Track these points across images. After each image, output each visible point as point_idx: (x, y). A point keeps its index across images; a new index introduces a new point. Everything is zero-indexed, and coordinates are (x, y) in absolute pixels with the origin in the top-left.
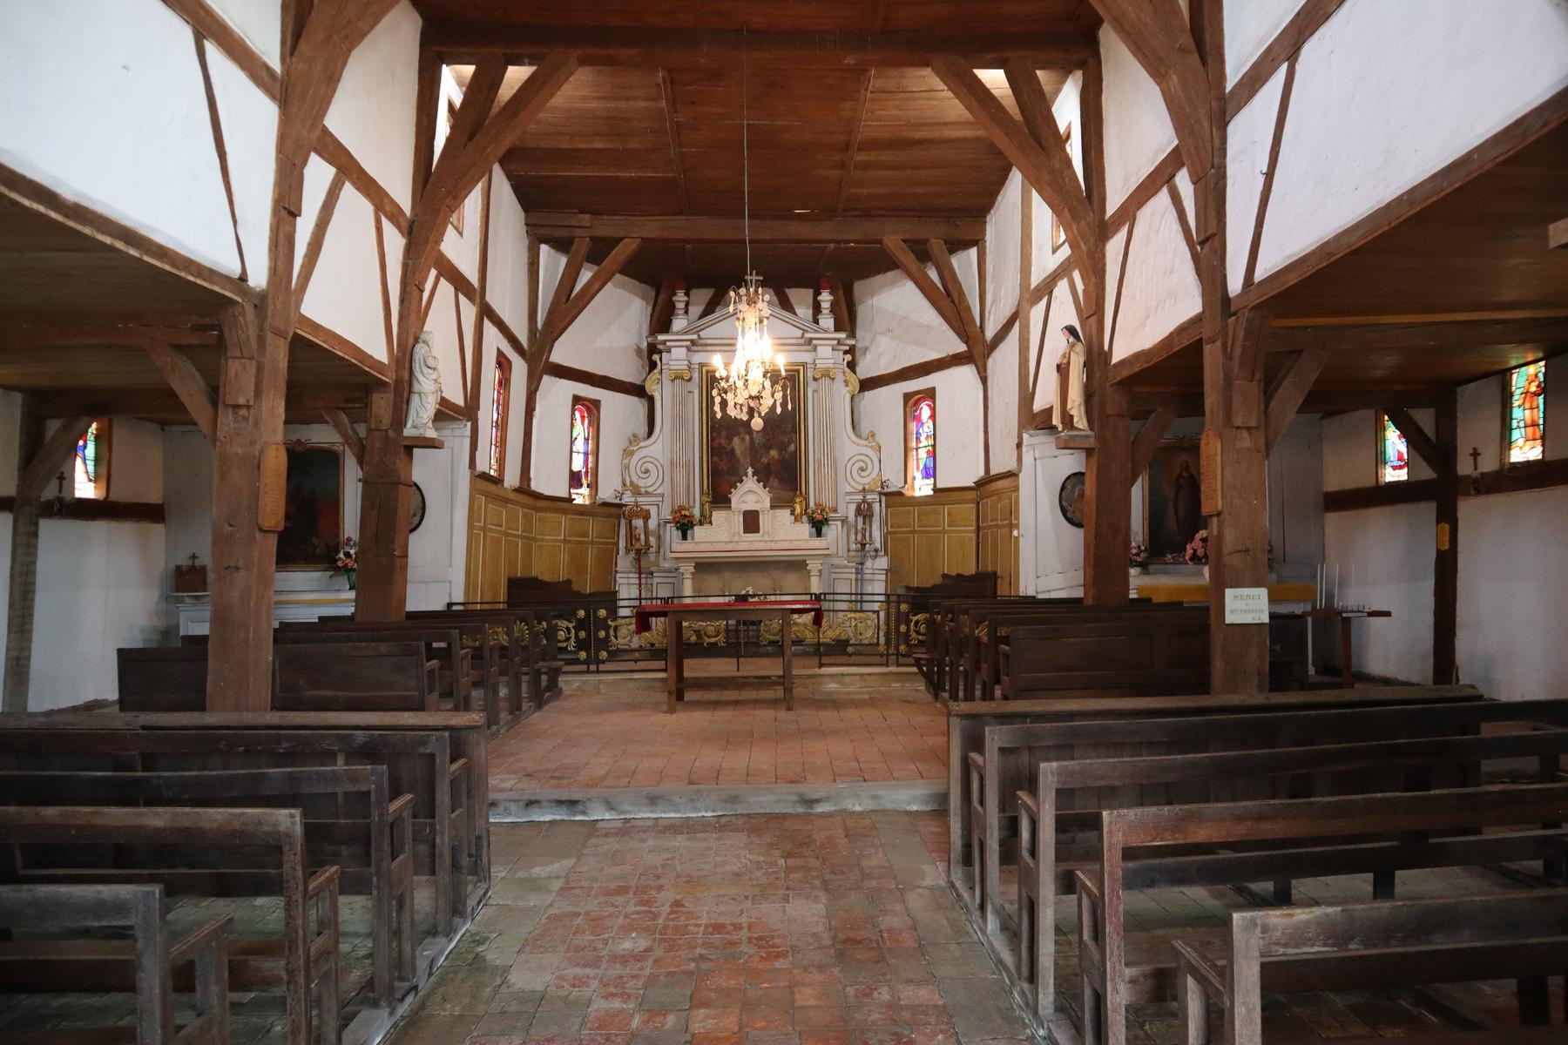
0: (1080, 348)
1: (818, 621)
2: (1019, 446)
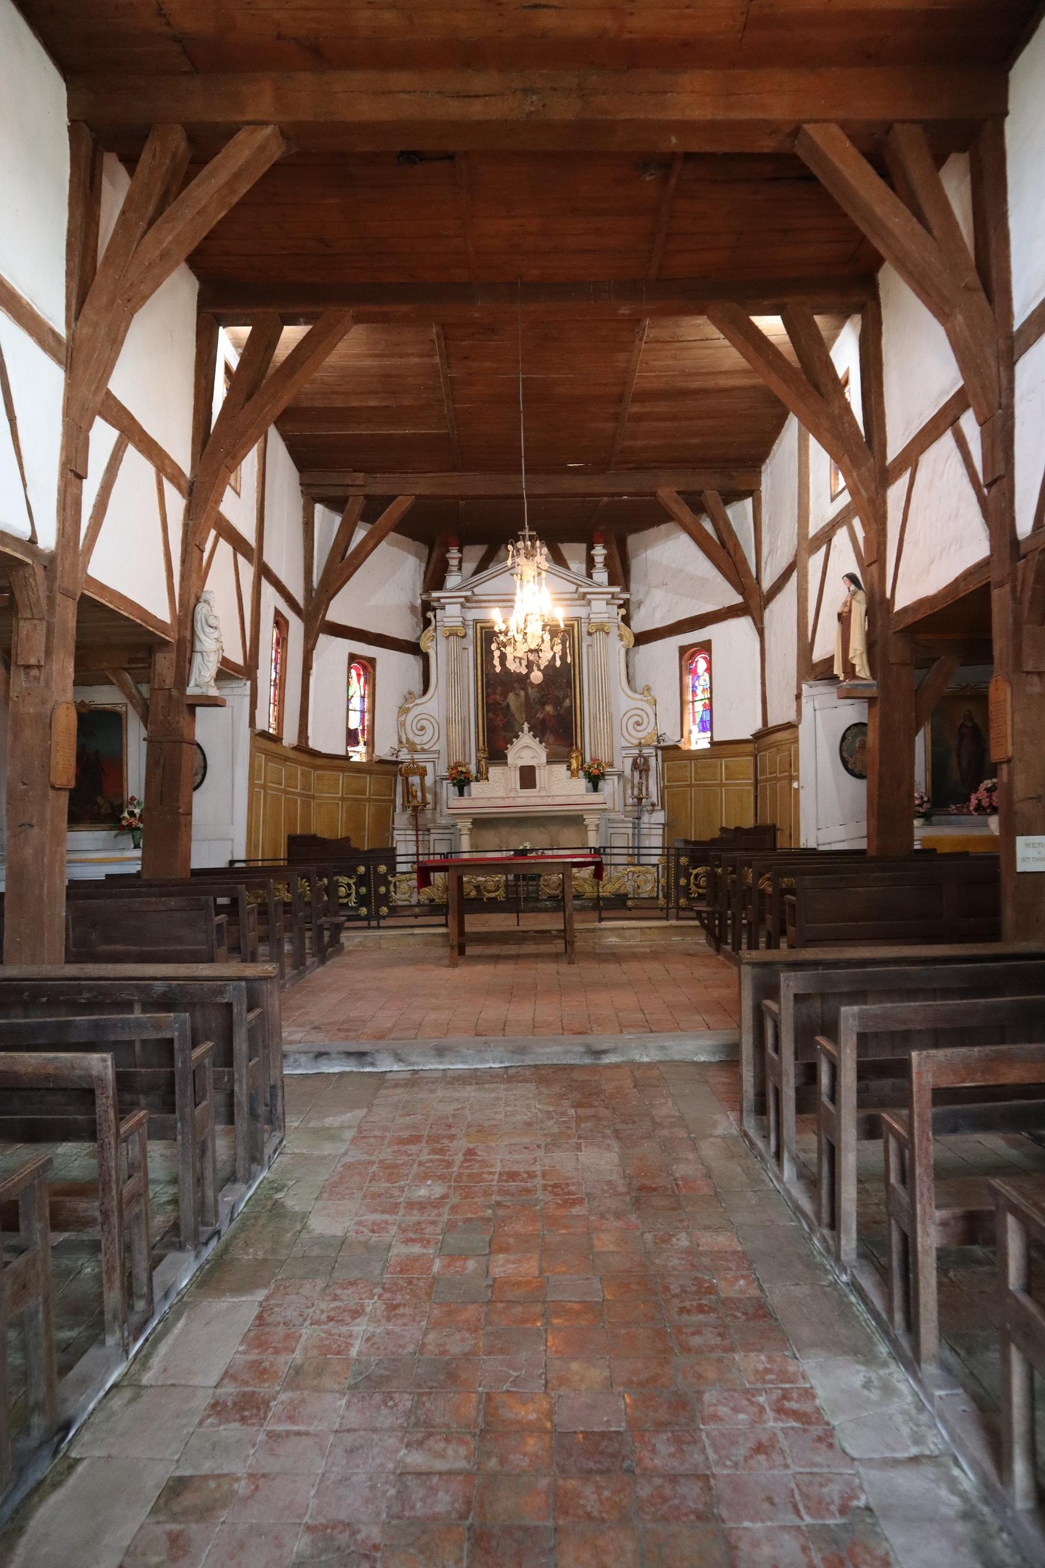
0: (861, 596)
1: (598, 874)
2: (798, 697)
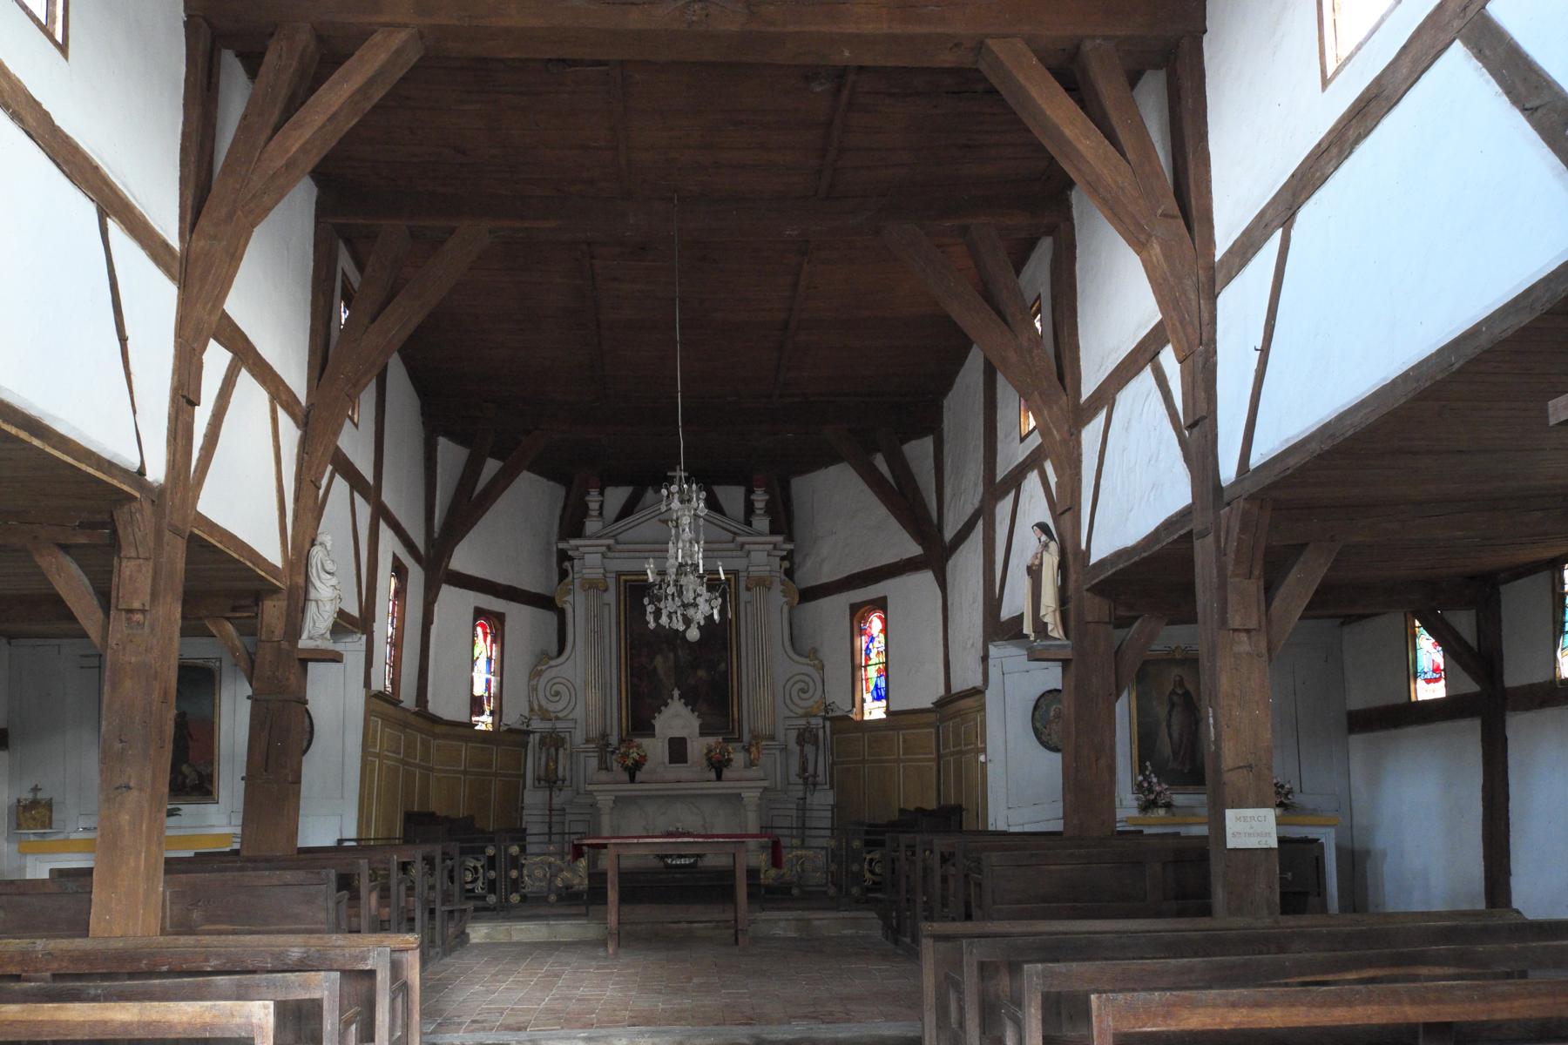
0: (1053, 546)
2: (985, 658)
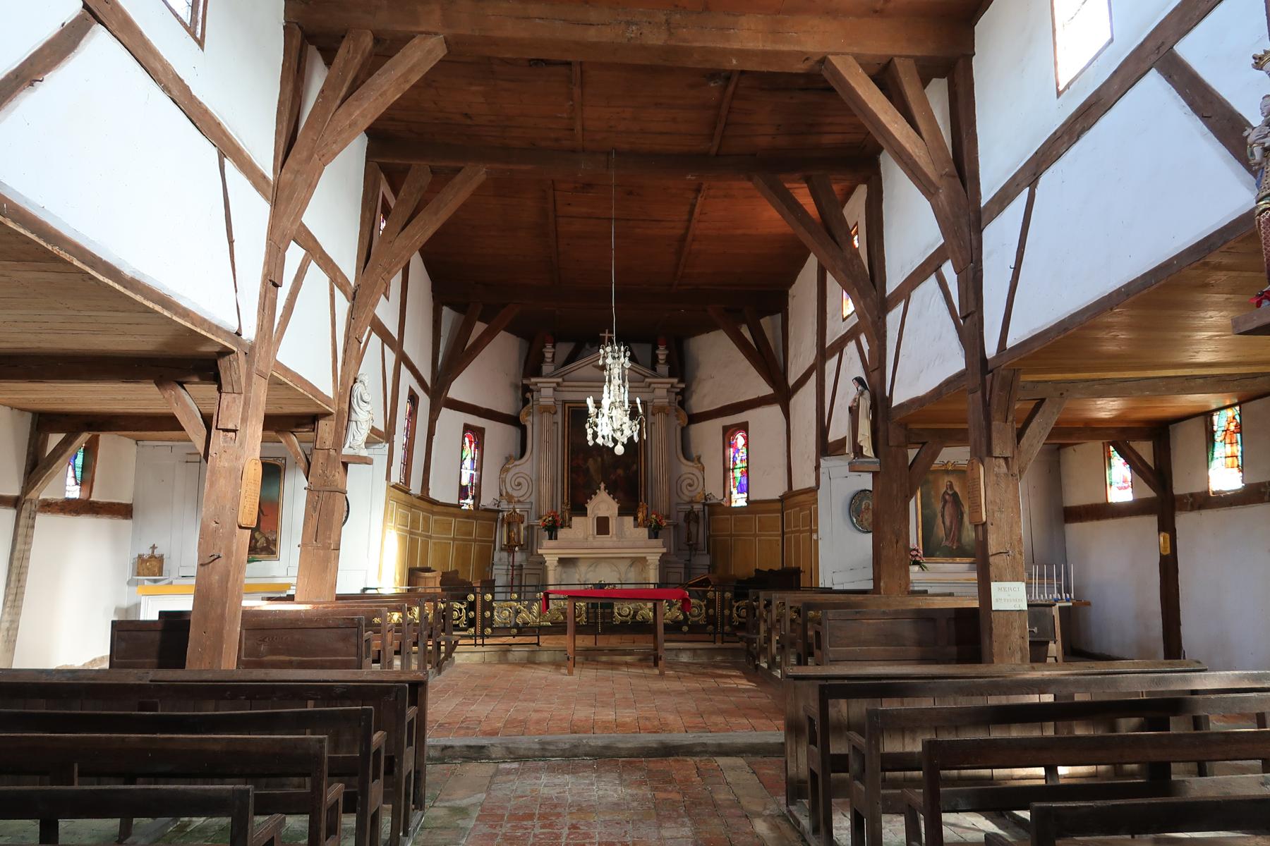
0: (867, 394)
2: (817, 468)
